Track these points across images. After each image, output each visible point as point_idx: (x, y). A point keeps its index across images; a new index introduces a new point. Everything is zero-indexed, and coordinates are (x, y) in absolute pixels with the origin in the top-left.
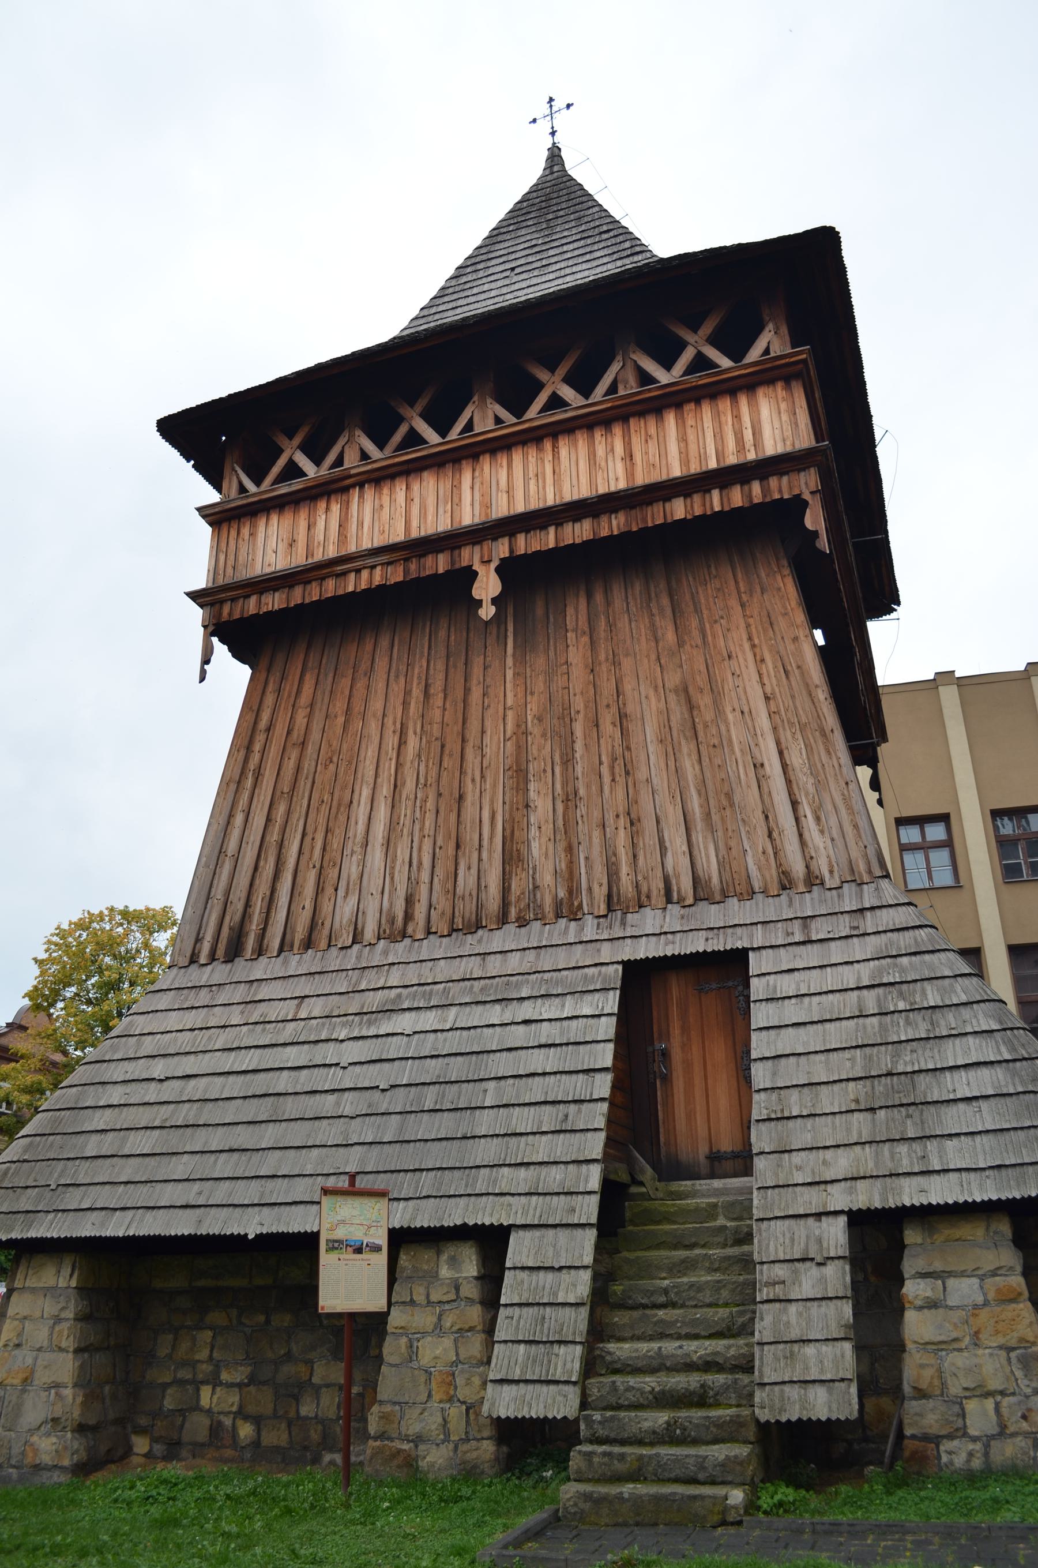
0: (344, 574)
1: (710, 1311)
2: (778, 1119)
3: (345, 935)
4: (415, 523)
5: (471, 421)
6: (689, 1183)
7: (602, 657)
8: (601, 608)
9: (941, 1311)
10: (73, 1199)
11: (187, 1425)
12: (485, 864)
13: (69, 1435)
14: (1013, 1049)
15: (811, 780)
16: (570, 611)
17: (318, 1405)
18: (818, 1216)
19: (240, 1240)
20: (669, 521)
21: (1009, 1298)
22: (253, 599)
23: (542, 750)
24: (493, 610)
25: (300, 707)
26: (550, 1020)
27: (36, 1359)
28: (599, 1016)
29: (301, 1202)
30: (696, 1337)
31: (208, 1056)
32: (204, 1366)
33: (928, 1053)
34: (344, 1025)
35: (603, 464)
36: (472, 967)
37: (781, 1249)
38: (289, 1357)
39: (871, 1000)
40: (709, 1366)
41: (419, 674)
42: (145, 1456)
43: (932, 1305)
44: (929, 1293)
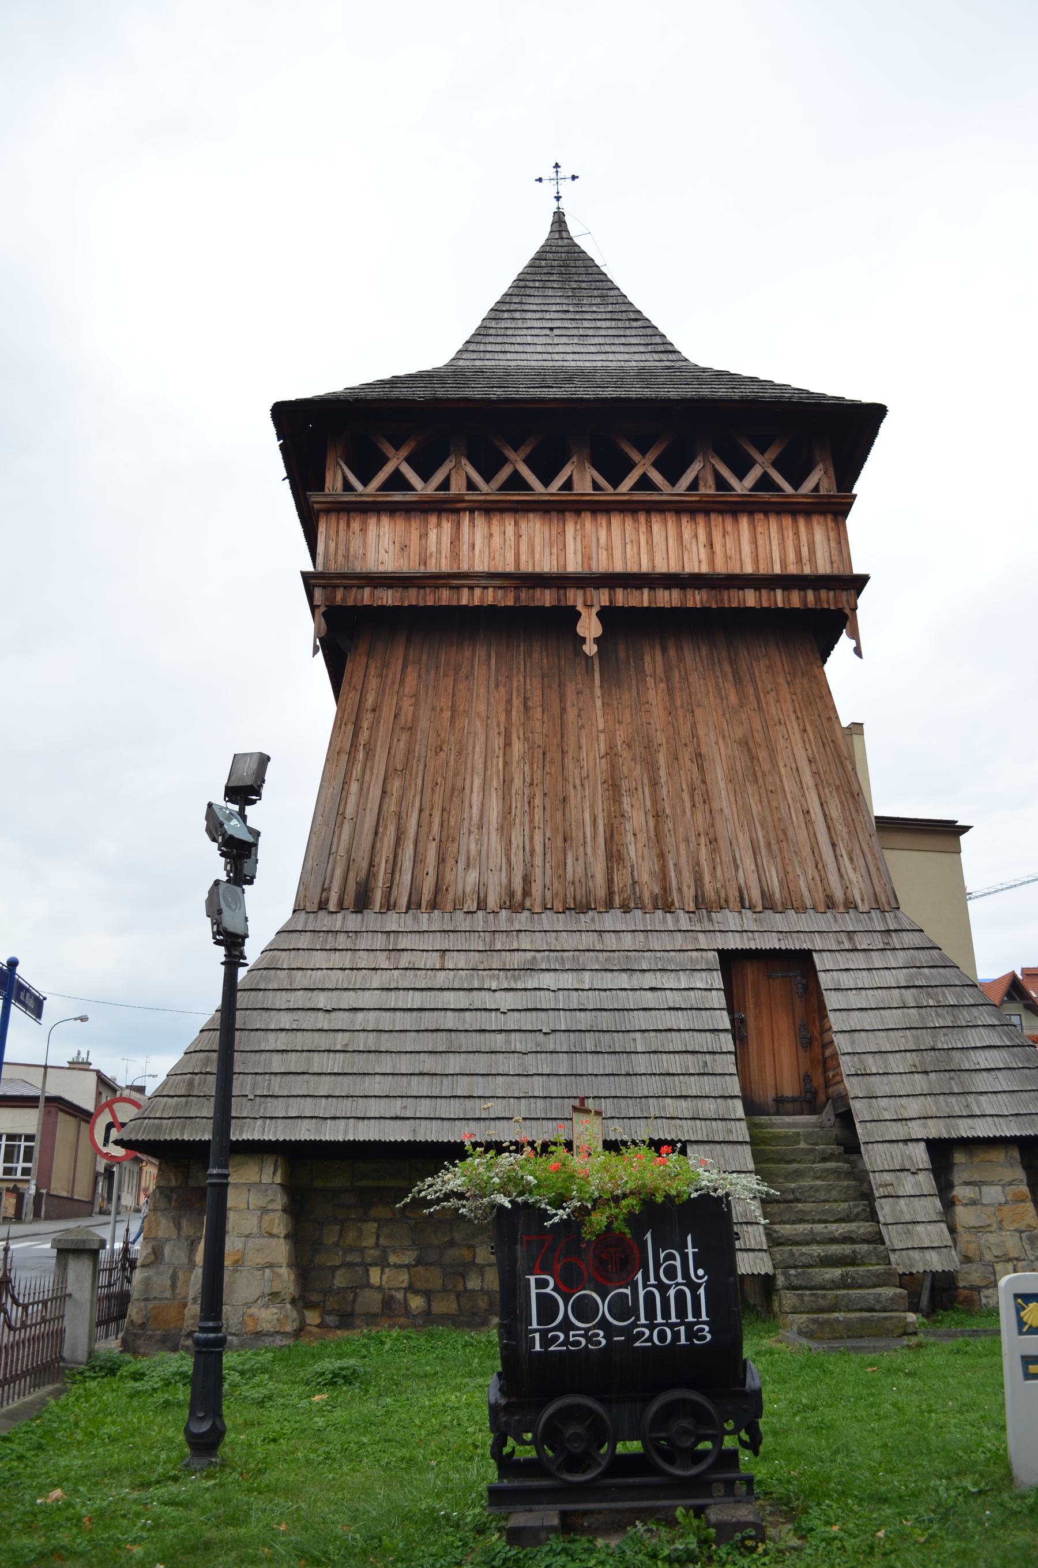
0: (458, 587)
1: (835, 1205)
2: (863, 1075)
3: (469, 902)
4: (523, 558)
5: (570, 480)
6: (767, 1118)
7: (678, 703)
8: (674, 662)
9: (979, 1207)
10: (277, 1108)
11: (360, 1299)
12: (590, 858)
13: (288, 1306)
15: (845, 830)
16: (647, 659)
17: (483, 1280)
18: (906, 1141)
20: (742, 606)
21: (1020, 1200)
22: (367, 591)
23: (633, 773)
24: (595, 649)
25: (404, 695)
26: (671, 989)
27: (245, 1244)
28: (710, 990)
29: (503, 1118)
30: (826, 1221)
31: (367, 993)
32: (372, 1252)
33: (955, 1037)
34: (493, 977)
35: (688, 546)
36: (589, 940)
37: (885, 1163)
38: (452, 1243)
39: (909, 996)
40: (846, 1239)
41: (518, 687)
42: (318, 1326)
43: (973, 1203)
44: (972, 1195)
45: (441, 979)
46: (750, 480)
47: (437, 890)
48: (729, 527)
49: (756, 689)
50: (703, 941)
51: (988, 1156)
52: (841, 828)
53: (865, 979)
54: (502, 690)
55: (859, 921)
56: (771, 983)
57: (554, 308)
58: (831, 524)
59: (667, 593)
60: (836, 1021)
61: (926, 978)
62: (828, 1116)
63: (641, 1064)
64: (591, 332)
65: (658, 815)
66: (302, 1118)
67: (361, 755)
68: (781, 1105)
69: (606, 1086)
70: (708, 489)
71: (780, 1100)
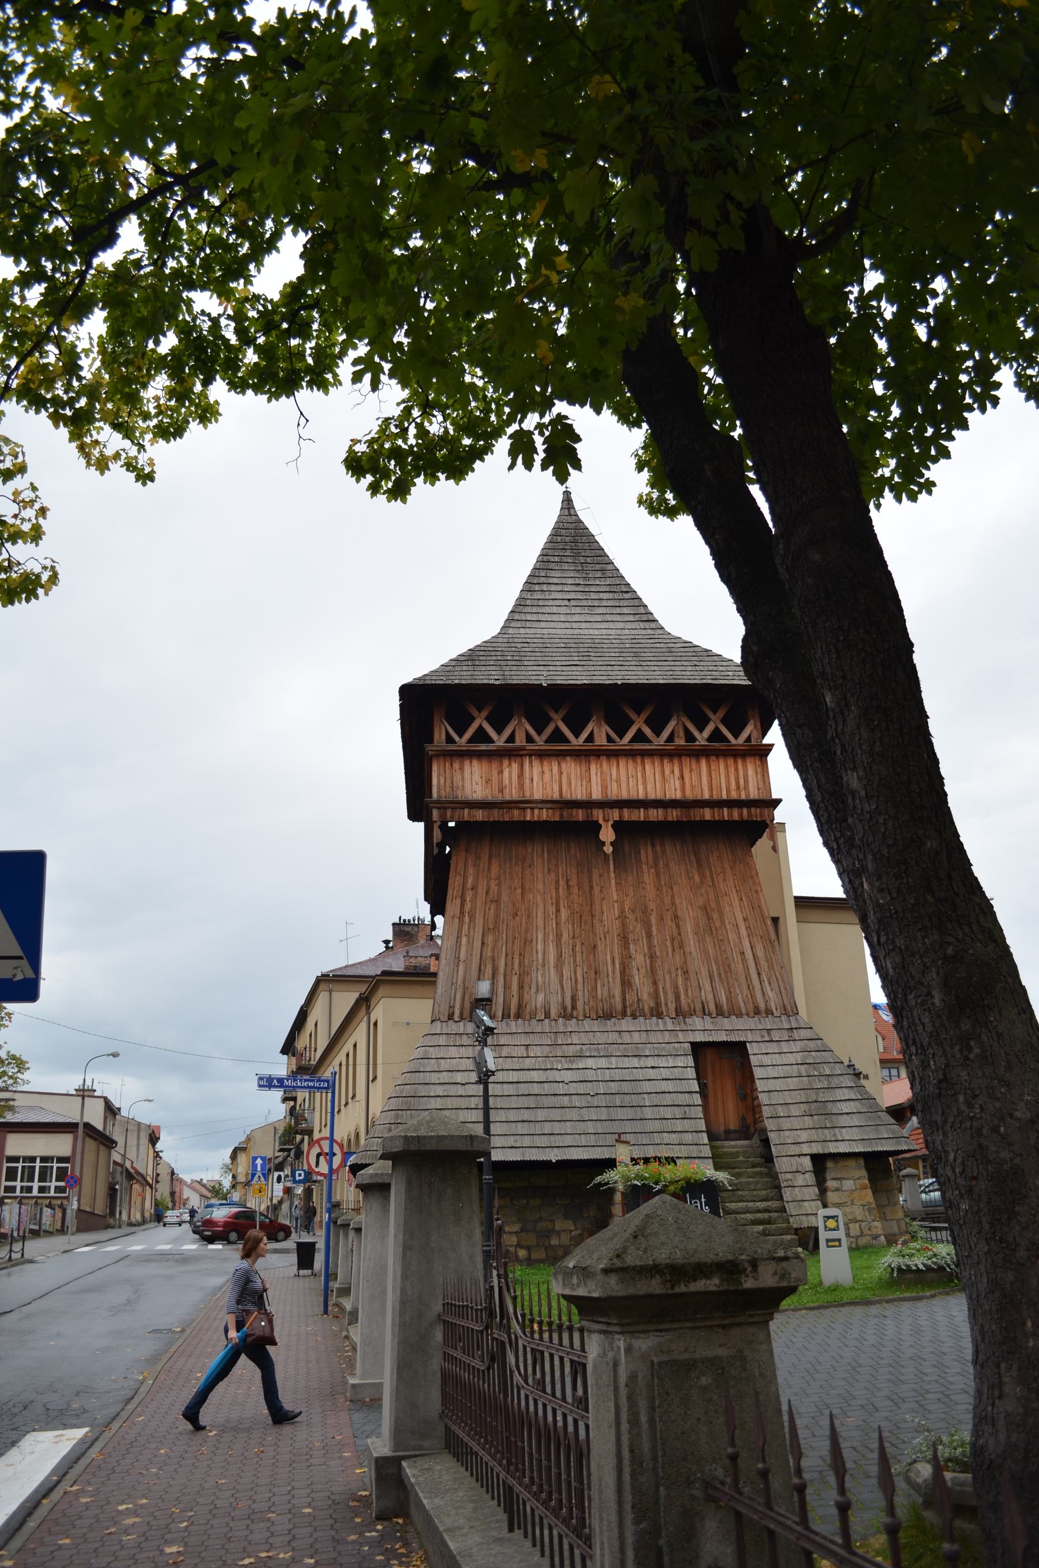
4: (564, 788)
5: (591, 734)
7: (663, 883)
12: (611, 985)
14: (861, 1095)
16: (643, 852)
18: (799, 1156)
19: (546, 1165)
22: (466, 811)
23: (637, 929)
24: (611, 849)
34: (558, 1061)
36: (613, 1037)
38: (541, 1219)
39: (803, 1069)
40: (766, 1210)
43: (837, 1190)
45: (528, 1063)
46: (707, 733)
47: (520, 1006)
48: (694, 766)
49: (711, 872)
50: (681, 1037)
51: (846, 1163)
52: (764, 964)
53: (777, 1059)
54: (553, 874)
55: (774, 1022)
56: (723, 1064)
57: (570, 581)
58: (758, 762)
59: (655, 811)
60: (760, 1085)
61: (814, 1058)
62: (756, 1140)
63: (649, 1113)
64: (596, 603)
65: (652, 957)
67: (467, 919)
68: (729, 1135)
69: (629, 1127)
70: (680, 741)
71: (727, 1132)
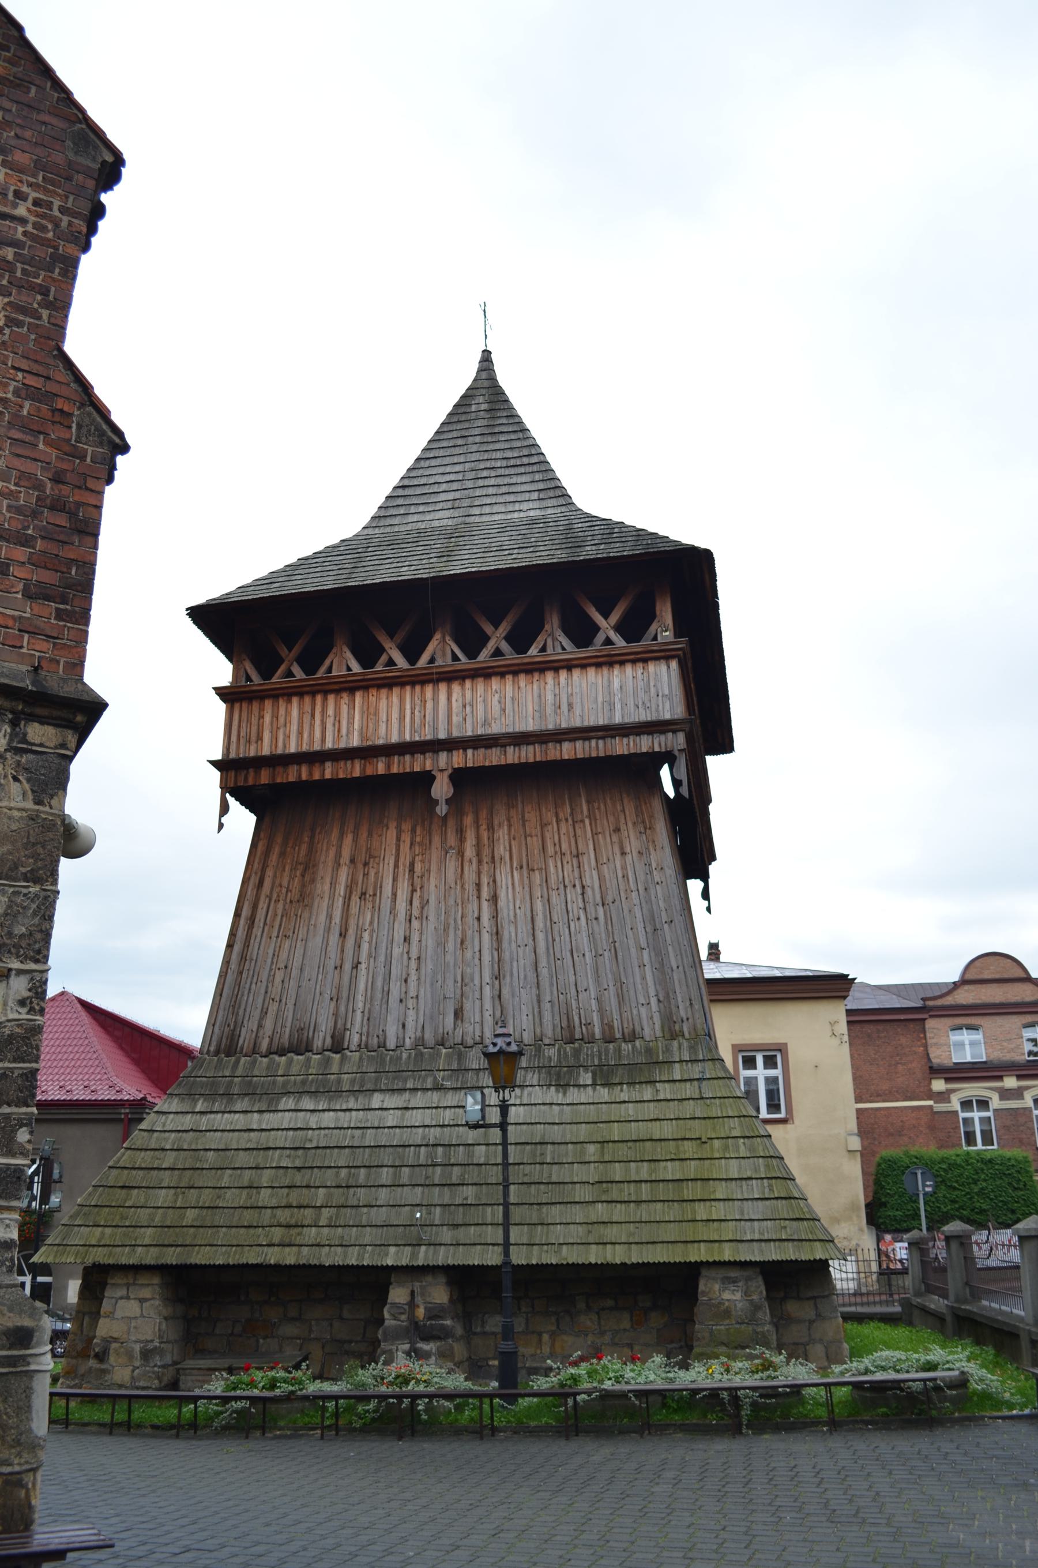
14: (771, 1190)
66: (612, 1223)
